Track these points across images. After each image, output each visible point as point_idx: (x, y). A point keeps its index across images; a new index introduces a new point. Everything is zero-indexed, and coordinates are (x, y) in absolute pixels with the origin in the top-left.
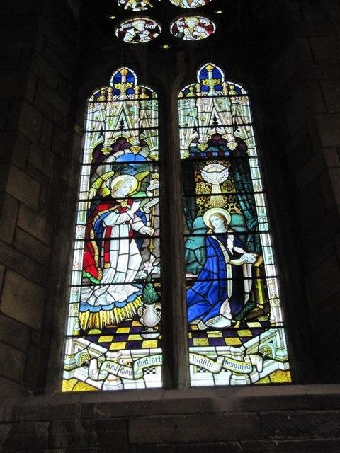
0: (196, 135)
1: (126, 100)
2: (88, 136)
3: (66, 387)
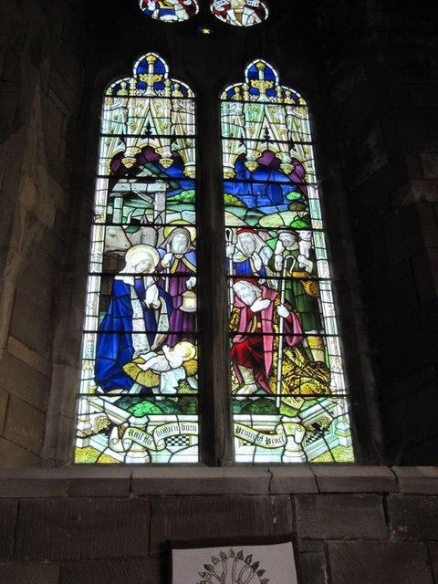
0: (122, 147)
1: (153, 97)
2: (104, 140)
3: (81, 458)
